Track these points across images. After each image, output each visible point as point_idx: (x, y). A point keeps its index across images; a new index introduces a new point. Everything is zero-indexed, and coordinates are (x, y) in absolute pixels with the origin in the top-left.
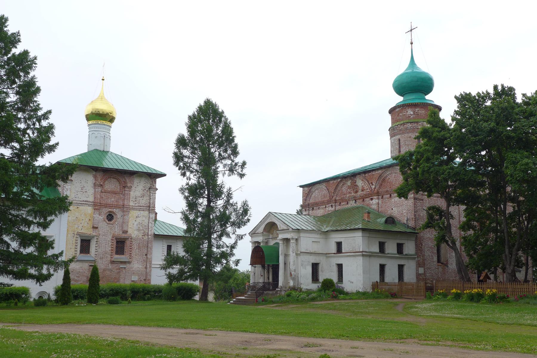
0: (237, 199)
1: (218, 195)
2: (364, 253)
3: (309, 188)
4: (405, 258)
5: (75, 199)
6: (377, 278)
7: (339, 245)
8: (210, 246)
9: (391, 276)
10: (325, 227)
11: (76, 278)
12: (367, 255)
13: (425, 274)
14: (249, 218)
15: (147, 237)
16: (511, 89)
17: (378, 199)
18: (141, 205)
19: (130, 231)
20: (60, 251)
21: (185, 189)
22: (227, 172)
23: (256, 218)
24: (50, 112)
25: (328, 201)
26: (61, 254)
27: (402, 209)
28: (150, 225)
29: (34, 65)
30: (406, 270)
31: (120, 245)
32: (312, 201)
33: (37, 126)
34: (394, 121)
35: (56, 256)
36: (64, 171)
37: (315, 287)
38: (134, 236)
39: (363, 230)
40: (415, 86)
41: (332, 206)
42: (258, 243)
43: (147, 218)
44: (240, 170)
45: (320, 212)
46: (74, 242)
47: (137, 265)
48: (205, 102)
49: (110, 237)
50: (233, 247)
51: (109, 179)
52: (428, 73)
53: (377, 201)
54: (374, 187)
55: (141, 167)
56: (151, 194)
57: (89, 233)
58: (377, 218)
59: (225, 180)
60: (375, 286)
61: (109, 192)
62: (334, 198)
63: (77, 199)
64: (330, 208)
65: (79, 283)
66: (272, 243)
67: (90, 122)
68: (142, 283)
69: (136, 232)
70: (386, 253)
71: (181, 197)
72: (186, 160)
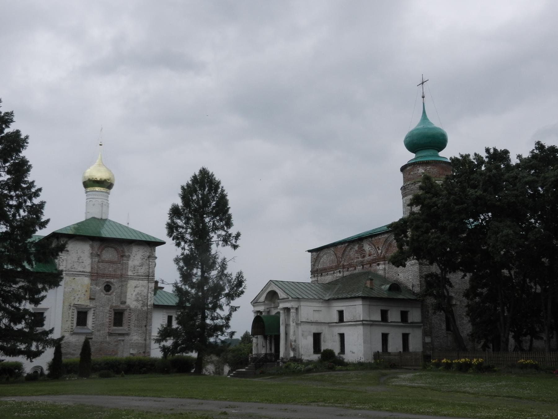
0: (232, 270)
1: (212, 267)
2: (364, 322)
3: (317, 252)
4: (409, 327)
5: (71, 270)
6: (379, 348)
7: (341, 313)
8: (204, 318)
9: (395, 345)
10: (328, 295)
11: (72, 352)
12: (368, 324)
13: (432, 343)
14: (244, 290)
15: (146, 308)
16: (506, 152)
17: (385, 264)
18: (140, 274)
19: (128, 302)
20: (51, 328)
21: (180, 259)
22: (221, 243)
23: (253, 288)
24: (40, 190)
25: (336, 266)
26: (51, 331)
27: (410, 274)
28: (149, 295)
29: (25, 144)
30: (410, 338)
31: (118, 317)
32: (320, 266)
33: (29, 204)
34: (406, 180)
35: (46, 333)
36: (60, 240)
37: (316, 357)
38: (132, 306)
39: (363, 298)
40: (426, 142)
41: (340, 272)
42: (261, 312)
43: (147, 288)
44: (233, 241)
45: (328, 278)
46: (70, 314)
47: (136, 337)
48: (201, 171)
49: (108, 308)
50: (228, 318)
51: (106, 249)
52: (440, 129)
53: (383, 266)
54: (380, 251)
55: (147, 237)
56: (151, 263)
57: (86, 304)
58: (382, 285)
59: (219, 250)
60: (376, 355)
61: (107, 262)
62: (341, 264)
63: (73, 270)
64: (338, 275)
65: (76, 356)
66: (274, 312)
67: (89, 189)
68: (141, 356)
69: (135, 303)
70: (389, 321)
71: (175, 267)
72: (180, 230)
